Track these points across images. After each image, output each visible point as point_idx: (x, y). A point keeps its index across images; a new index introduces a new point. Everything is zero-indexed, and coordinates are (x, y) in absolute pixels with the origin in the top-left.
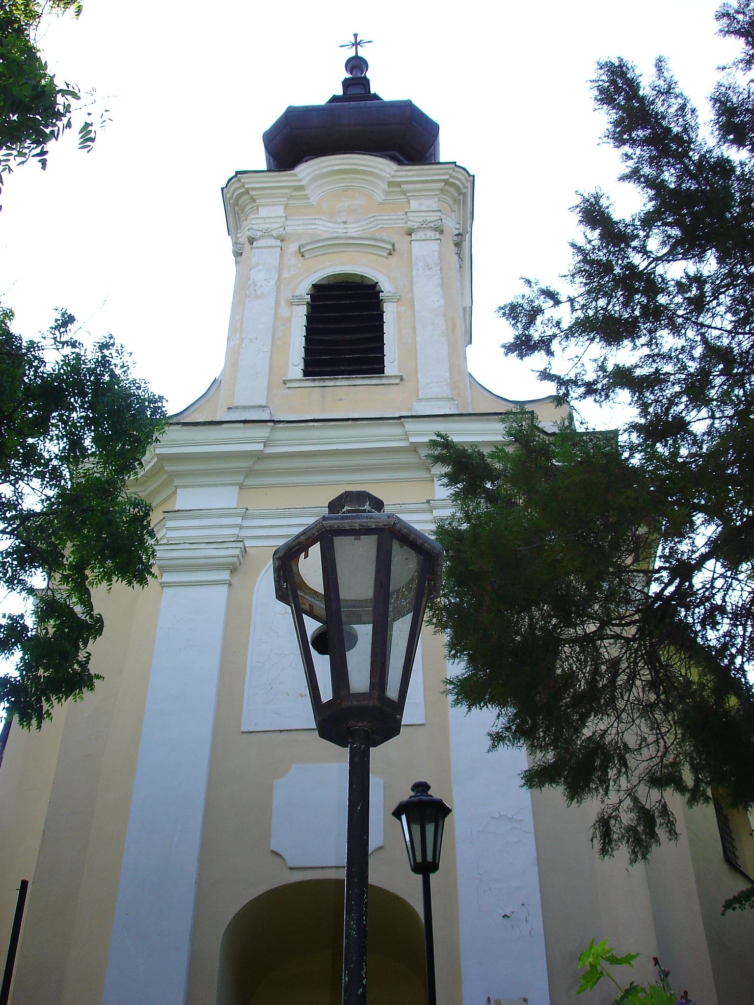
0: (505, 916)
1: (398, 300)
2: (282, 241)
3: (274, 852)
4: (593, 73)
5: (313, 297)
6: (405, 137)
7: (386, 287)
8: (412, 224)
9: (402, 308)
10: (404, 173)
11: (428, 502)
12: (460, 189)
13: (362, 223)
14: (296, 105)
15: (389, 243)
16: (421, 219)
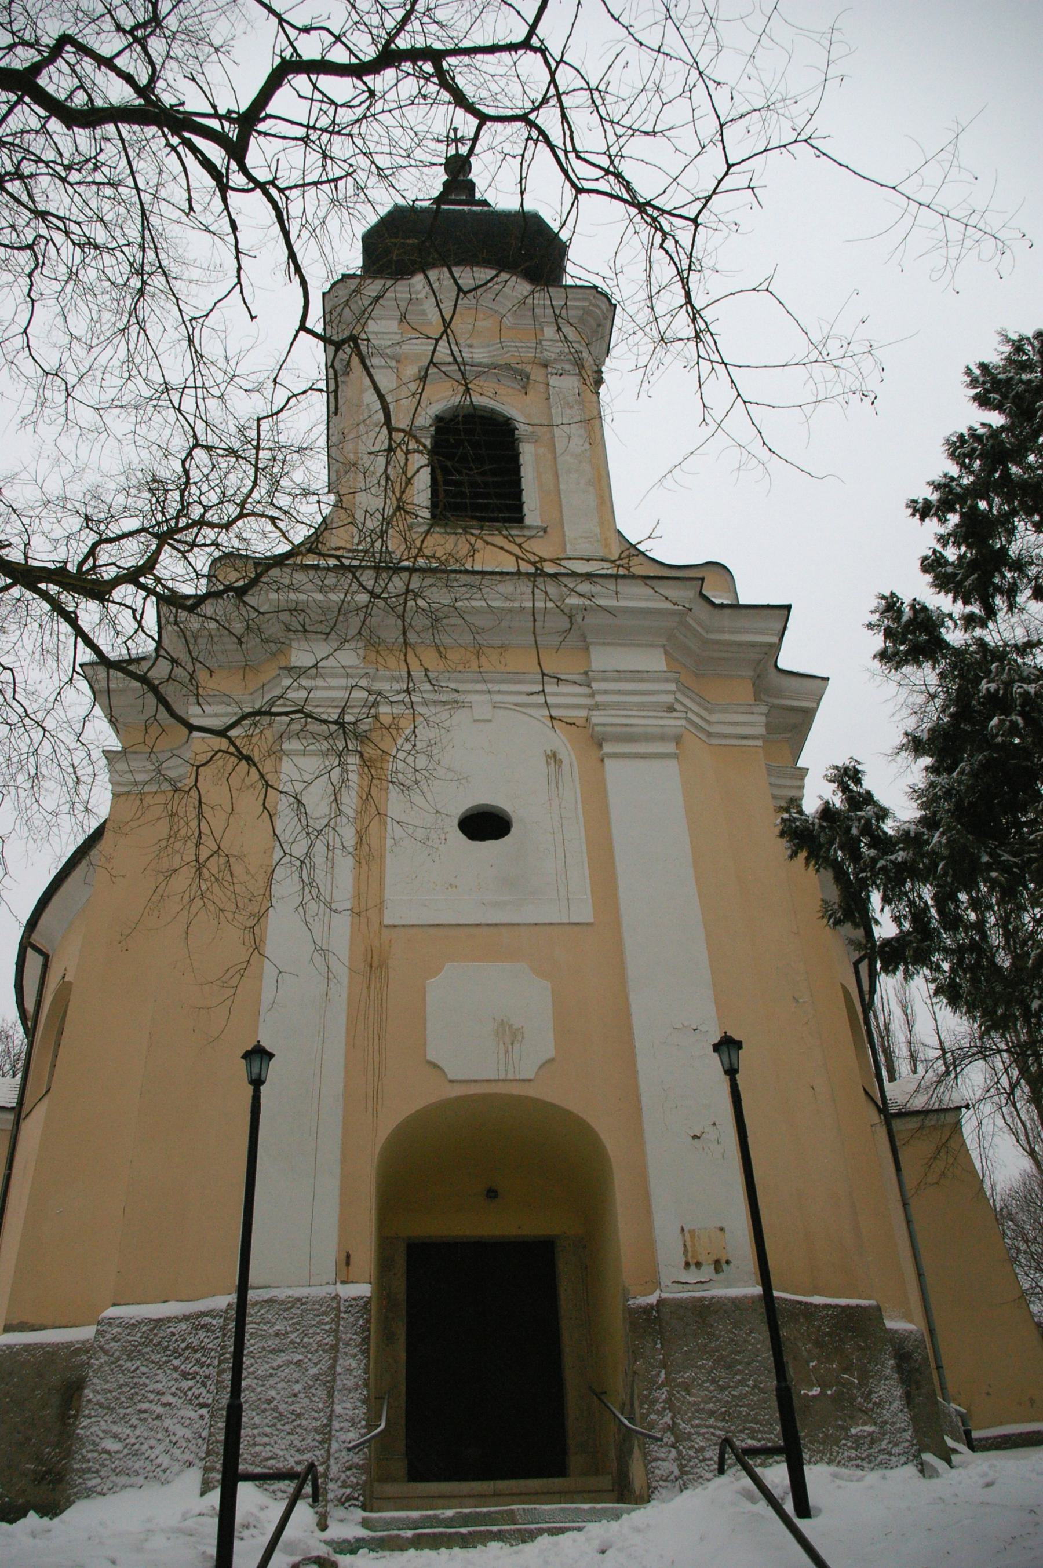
0: (695, 1137)
1: (535, 439)
2: (398, 361)
3: (430, 1063)
4: (875, 603)
5: (437, 430)
6: (529, 249)
9: (541, 451)
11: (586, 673)
13: (491, 348)
14: (338, 79)
15: (857, 973)
16: (558, 351)
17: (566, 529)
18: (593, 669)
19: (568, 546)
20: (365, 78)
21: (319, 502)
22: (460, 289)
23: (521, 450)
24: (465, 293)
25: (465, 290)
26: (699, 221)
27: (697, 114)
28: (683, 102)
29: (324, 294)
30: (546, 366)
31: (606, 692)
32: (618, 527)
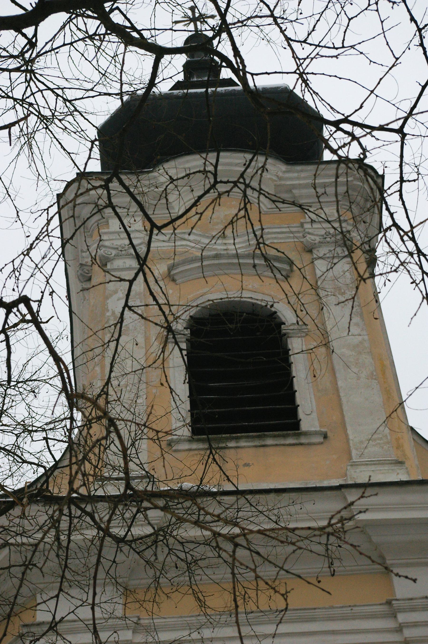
6: (286, 126)
7: (287, 315)
8: (313, 237)
10: (296, 175)
11: (389, 603)
12: (366, 188)
17: (349, 432)
18: (398, 596)
19: (354, 453)
20: (24, 31)
21: (46, 439)
22: (153, 225)
23: (290, 346)
24: (160, 228)
25: (159, 225)
26: (405, 130)
27: (386, 25)
28: (371, 15)
29: (58, 195)
30: (310, 251)
31: (415, 625)
32: (411, 424)
